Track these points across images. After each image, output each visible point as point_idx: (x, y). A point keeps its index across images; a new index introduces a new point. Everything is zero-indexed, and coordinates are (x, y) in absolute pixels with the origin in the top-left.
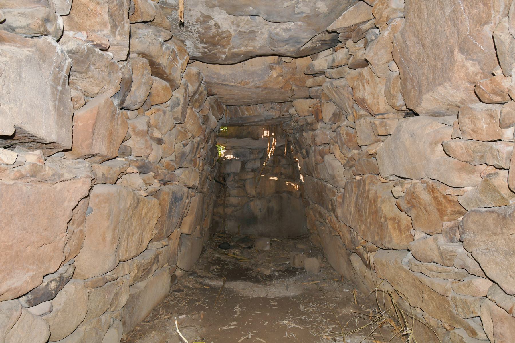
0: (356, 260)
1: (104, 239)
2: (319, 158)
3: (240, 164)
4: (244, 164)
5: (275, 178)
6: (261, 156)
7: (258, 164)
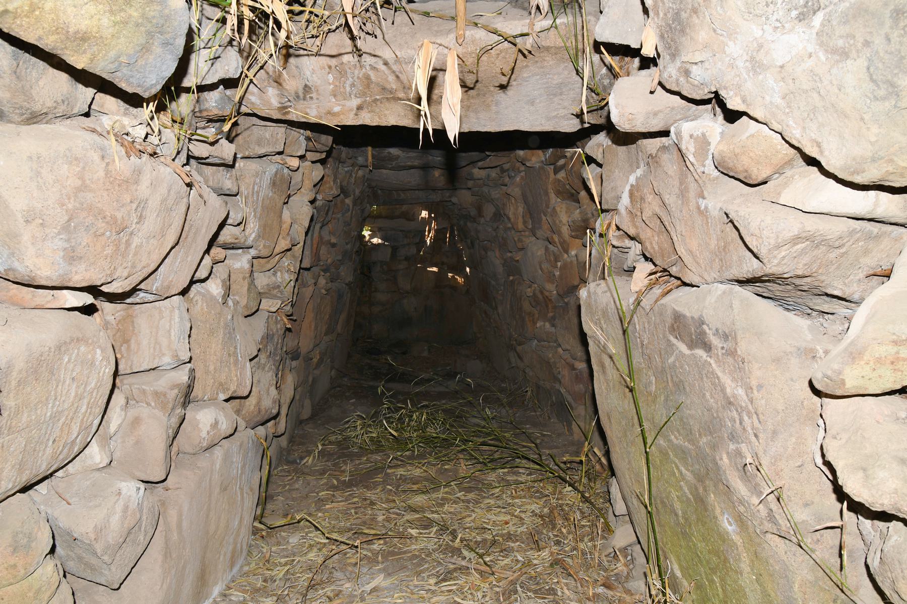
0: (512, 355)
1: (310, 327)
2: (483, 253)
3: (390, 250)
4: (395, 249)
5: (435, 269)
6: (418, 241)
7: (413, 250)
